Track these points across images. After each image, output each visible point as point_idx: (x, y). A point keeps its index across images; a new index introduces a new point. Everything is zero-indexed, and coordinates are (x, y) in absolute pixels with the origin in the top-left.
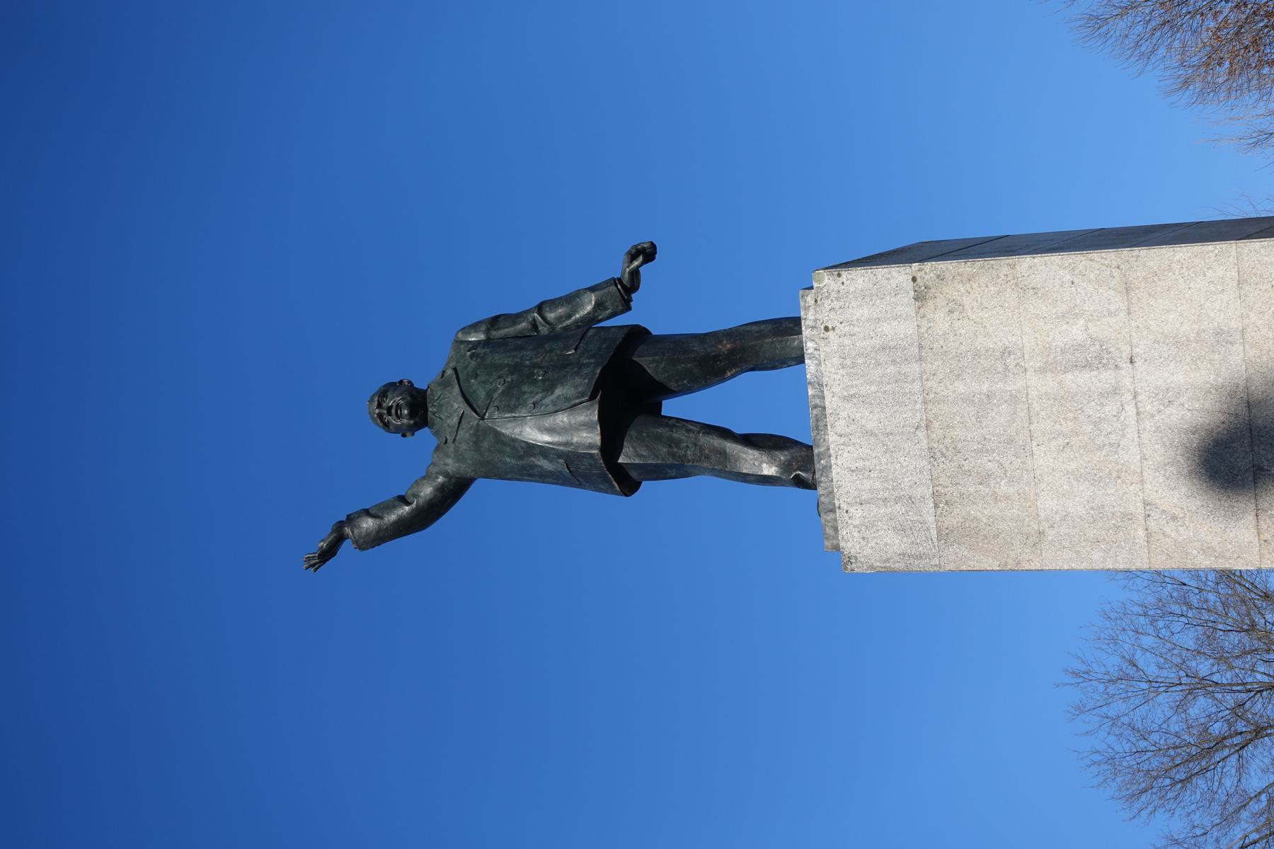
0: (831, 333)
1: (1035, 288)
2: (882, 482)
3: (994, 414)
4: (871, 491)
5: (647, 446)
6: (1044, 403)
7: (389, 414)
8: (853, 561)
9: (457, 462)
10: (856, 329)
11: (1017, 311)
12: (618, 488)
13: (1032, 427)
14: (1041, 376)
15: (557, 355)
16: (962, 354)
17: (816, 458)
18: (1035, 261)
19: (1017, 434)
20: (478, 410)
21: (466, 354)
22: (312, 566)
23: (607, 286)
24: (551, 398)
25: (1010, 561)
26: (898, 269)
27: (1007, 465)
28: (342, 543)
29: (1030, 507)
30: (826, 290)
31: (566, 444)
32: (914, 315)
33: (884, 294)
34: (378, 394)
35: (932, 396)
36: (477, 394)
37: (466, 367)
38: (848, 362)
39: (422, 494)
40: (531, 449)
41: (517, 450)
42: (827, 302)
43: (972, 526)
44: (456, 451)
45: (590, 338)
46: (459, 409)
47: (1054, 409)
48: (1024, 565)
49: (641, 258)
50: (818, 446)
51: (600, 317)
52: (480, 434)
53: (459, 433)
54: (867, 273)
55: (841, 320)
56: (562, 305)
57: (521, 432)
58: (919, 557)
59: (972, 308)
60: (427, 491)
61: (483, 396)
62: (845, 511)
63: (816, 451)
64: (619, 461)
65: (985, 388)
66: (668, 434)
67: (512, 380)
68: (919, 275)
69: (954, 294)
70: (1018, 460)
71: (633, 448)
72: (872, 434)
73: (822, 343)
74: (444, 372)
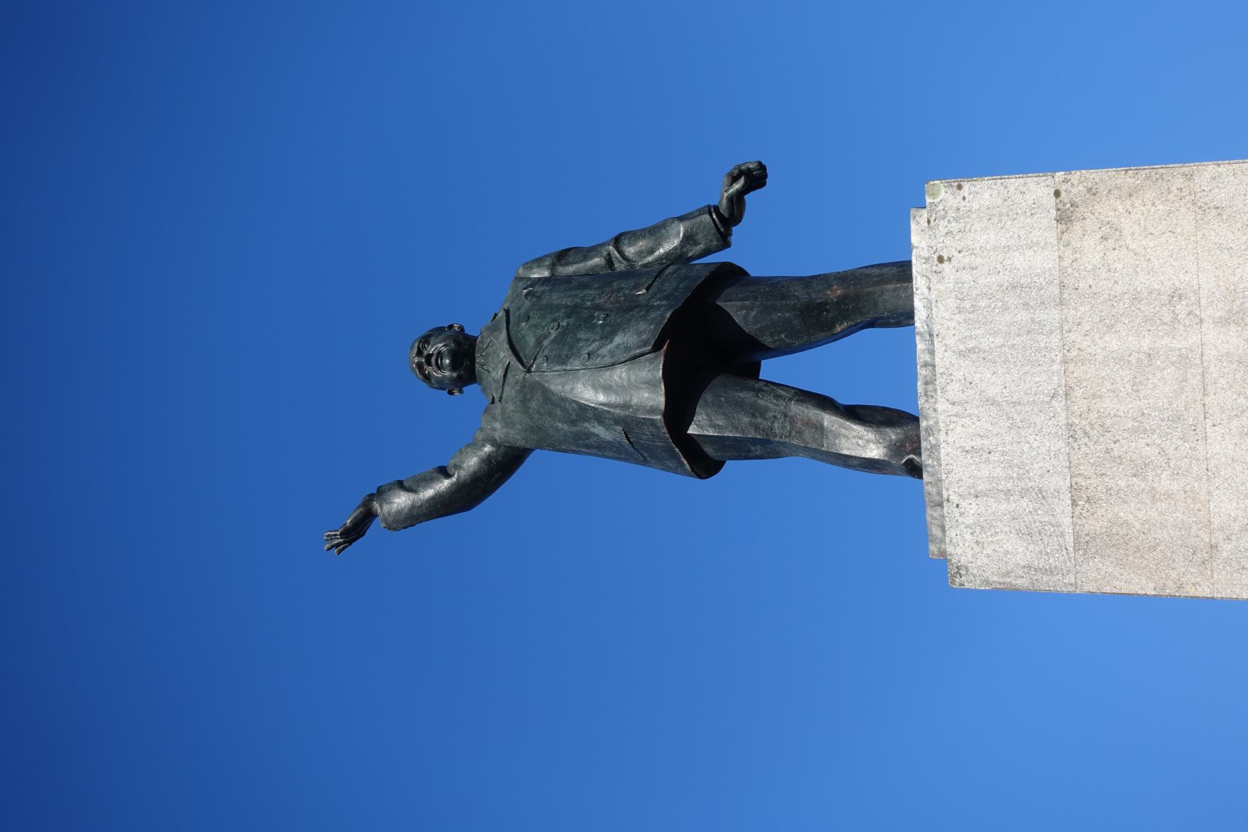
0: (946, 264)
1: (1218, 208)
2: (1004, 468)
3: (1156, 381)
4: (990, 479)
5: (724, 414)
6: (1225, 367)
7: (429, 364)
8: (963, 572)
9: (506, 427)
10: (979, 260)
11: (1192, 238)
12: (688, 467)
13: (1207, 400)
14: (1222, 330)
15: (625, 295)
16: (1116, 296)
17: (923, 433)
18: (1220, 169)
19: (1185, 409)
20: (525, 360)
21: (522, 292)
22: (337, 545)
23: (700, 215)
24: (609, 347)
25: (1170, 584)
26: (1036, 179)
27: (1171, 451)
28: (372, 521)
29: (1199, 510)
30: (941, 207)
31: (626, 406)
32: (1055, 242)
33: (1017, 214)
34: (419, 340)
35: (1074, 353)
36: (526, 341)
37: (519, 309)
38: (967, 304)
39: (465, 464)
40: (586, 413)
41: (568, 412)
42: (944, 223)
43: (1121, 533)
44: (503, 413)
45: (667, 275)
46: (505, 359)
47: (1238, 376)
48: (1188, 589)
49: (742, 181)
50: (926, 419)
51: (690, 254)
52: (528, 391)
53: (505, 389)
54: (995, 184)
55: (959, 248)
56: (644, 237)
57: (572, 389)
58: (1050, 571)
59: (1133, 234)
60: (472, 462)
61: (531, 343)
62: (955, 506)
63: (923, 424)
64: (690, 432)
65: (1146, 343)
66: (753, 399)
67: (568, 324)
68: (1064, 188)
69: (1110, 214)
70: (1186, 444)
71: (706, 415)
72: (994, 402)
73: (934, 279)
74: (496, 315)
